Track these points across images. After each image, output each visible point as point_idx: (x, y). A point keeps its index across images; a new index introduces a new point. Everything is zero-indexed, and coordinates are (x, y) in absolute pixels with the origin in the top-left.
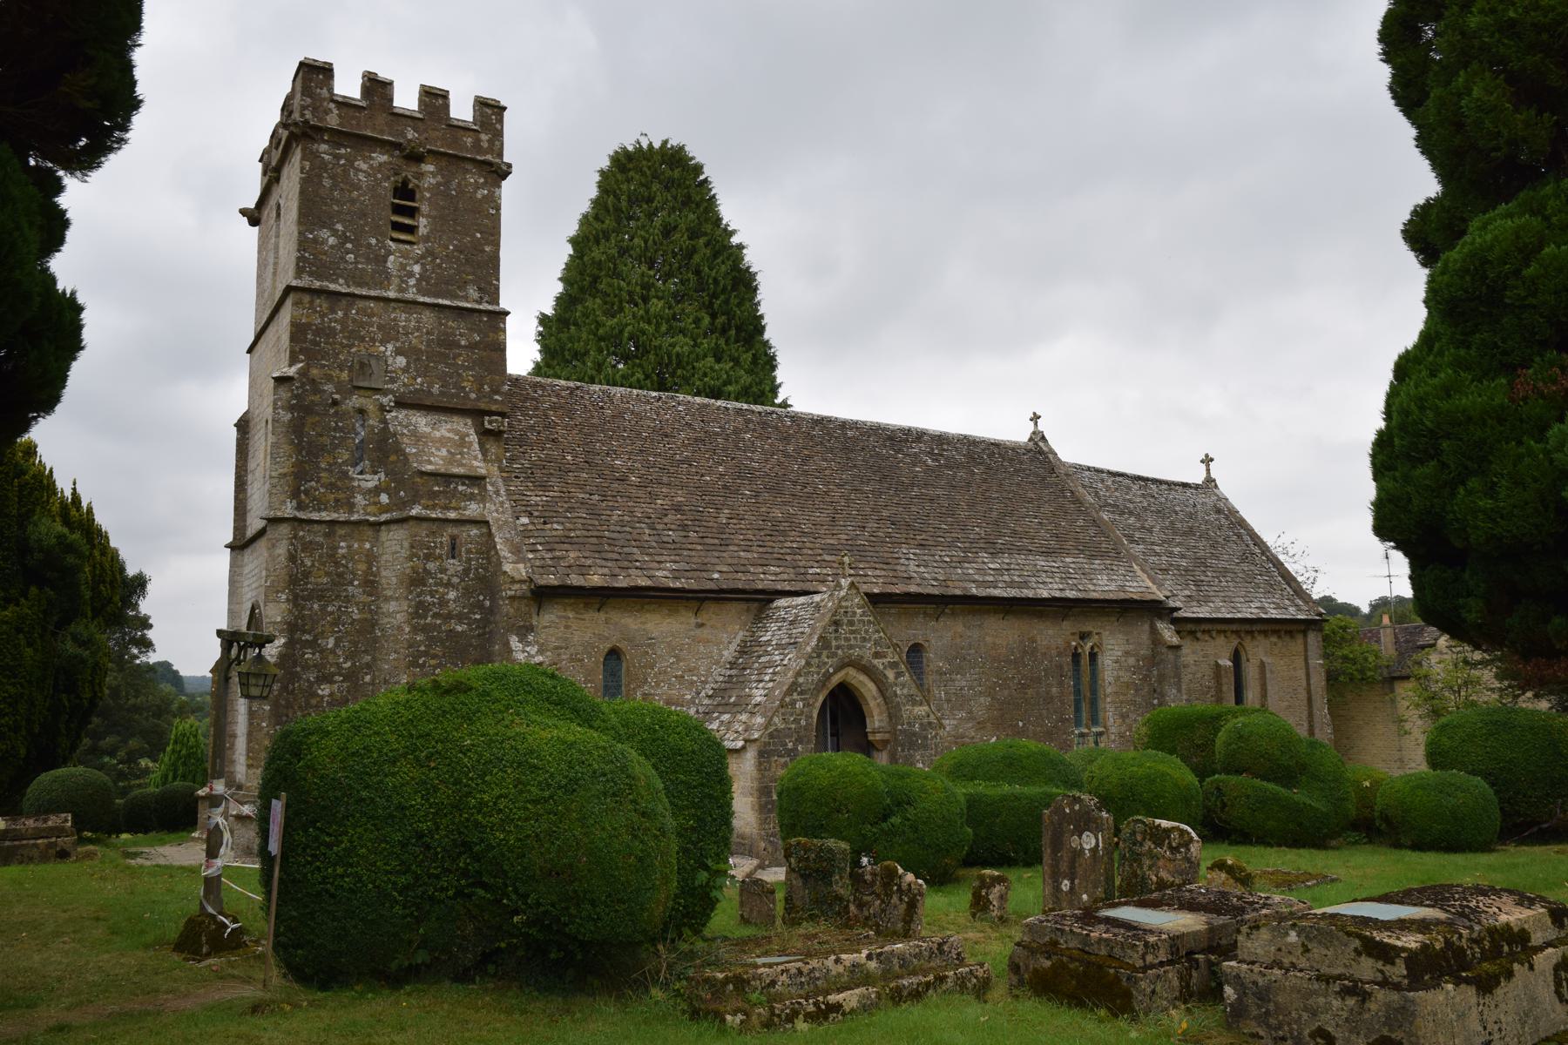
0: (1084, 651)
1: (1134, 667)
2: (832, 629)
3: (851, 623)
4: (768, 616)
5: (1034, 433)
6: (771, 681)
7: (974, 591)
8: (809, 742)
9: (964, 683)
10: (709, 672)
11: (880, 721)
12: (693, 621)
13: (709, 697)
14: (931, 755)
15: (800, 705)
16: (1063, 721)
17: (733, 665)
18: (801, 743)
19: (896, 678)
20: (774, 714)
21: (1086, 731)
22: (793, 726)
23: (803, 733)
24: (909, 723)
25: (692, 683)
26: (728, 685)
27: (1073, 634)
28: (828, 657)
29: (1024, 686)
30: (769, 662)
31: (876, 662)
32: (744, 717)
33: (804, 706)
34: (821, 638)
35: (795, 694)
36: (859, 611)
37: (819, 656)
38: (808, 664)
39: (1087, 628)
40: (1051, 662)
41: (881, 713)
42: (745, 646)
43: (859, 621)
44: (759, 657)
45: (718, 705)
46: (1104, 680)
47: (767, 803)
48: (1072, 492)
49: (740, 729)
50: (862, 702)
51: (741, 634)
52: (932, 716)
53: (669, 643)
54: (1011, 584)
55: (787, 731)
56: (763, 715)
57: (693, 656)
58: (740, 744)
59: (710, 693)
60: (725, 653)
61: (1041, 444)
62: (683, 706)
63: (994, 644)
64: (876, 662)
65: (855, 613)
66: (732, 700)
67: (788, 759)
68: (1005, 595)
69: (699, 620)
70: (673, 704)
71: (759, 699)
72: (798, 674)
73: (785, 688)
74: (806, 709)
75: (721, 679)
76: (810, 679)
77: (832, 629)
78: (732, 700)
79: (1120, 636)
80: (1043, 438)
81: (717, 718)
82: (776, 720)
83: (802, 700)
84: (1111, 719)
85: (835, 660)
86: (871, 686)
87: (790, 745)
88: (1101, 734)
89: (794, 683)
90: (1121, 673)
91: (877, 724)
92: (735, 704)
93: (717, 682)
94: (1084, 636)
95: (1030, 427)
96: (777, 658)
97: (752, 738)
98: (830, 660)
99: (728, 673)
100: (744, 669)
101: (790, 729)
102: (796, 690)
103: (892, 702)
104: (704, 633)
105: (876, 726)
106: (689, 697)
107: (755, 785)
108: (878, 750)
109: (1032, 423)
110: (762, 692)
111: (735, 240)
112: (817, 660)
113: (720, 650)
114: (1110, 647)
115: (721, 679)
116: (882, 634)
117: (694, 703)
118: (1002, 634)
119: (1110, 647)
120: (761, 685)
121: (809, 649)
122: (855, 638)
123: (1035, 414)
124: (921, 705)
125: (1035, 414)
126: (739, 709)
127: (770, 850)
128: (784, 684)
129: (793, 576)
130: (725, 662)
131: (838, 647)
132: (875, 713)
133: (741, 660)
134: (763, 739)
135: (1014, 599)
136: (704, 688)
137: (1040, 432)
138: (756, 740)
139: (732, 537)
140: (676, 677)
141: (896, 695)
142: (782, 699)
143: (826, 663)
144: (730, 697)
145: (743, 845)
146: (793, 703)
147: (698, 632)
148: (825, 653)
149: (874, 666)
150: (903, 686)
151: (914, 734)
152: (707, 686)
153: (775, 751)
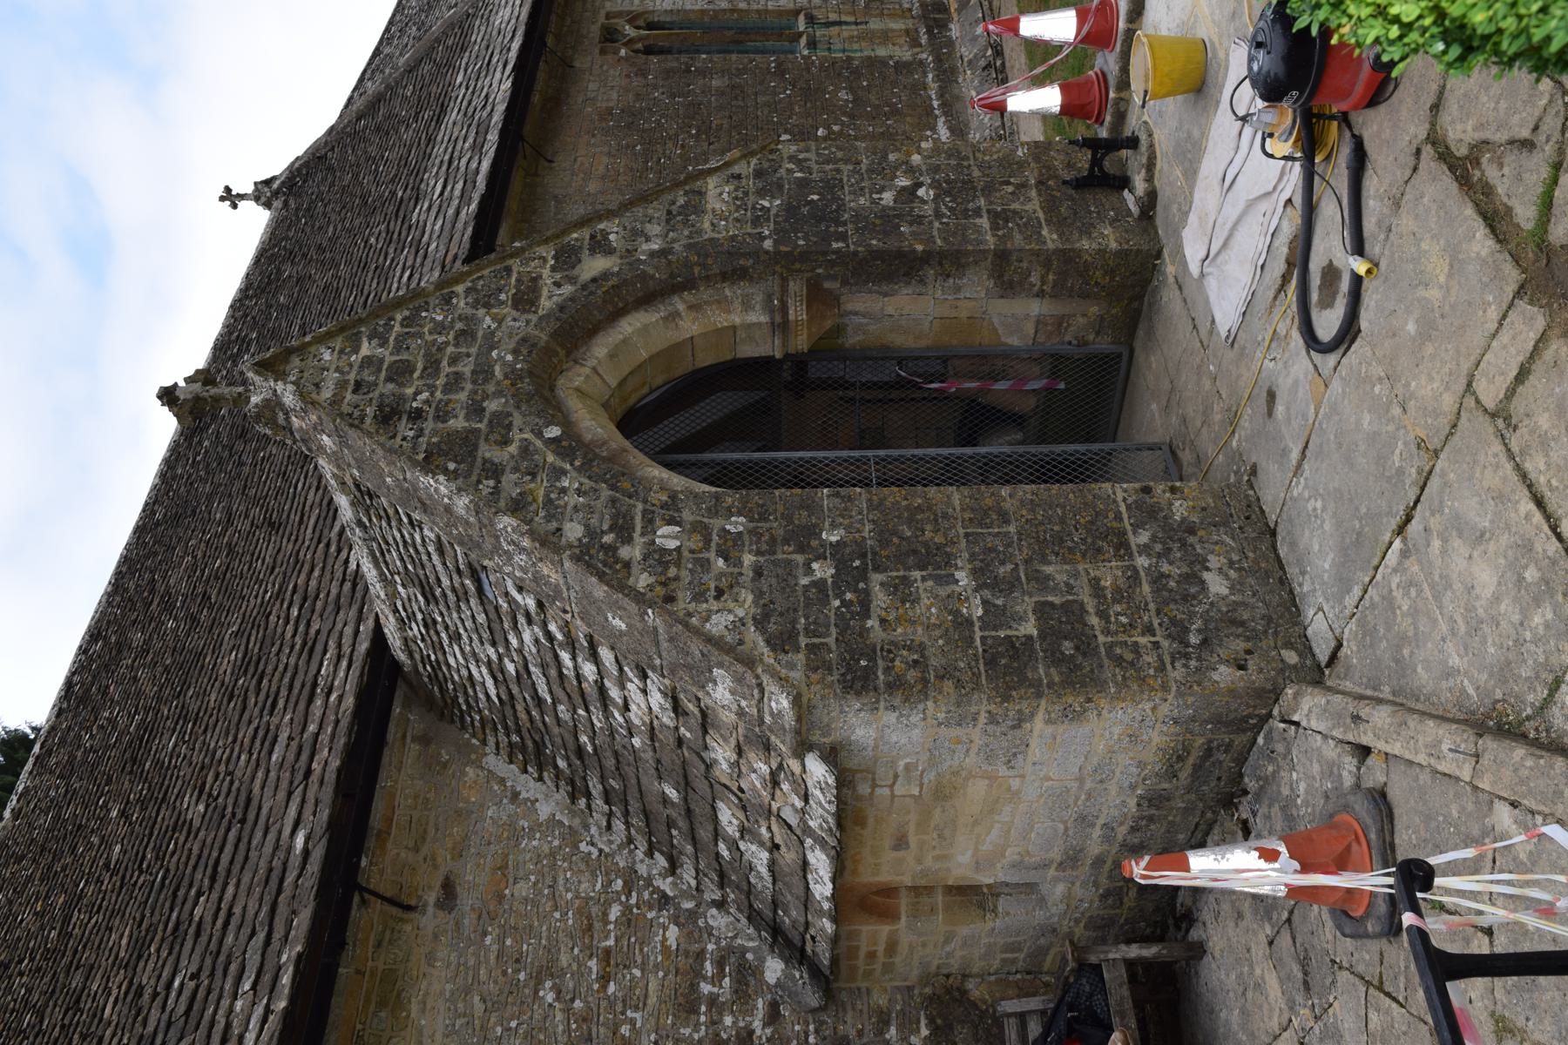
0: (640, 39)
2: (405, 429)
3: (400, 372)
4: (434, 677)
5: (257, 199)
6: (595, 657)
7: (473, 206)
8: (811, 507)
10: (600, 865)
11: (747, 306)
12: (430, 919)
13: (673, 868)
14: (854, 171)
15: (668, 537)
16: (781, 71)
17: (577, 791)
18: (813, 531)
19: (609, 251)
20: (697, 632)
21: (803, 40)
22: (748, 559)
23: (777, 527)
24: (756, 222)
25: (628, 920)
26: (634, 806)
28: (506, 442)
30: (544, 667)
31: (546, 304)
32: (722, 754)
33: (671, 521)
34: (429, 464)
35: (624, 552)
36: (365, 350)
37: (495, 471)
38: (517, 507)
40: (655, 87)
41: (724, 304)
42: (523, 748)
43: (398, 349)
44: (539, 701)
45: (694, 841)
46: (703, 12)
47: (1056, 659)
48: (359, 119)
49: (764, 768)
50: (683, 368)
51: (496, 763)
52: (736, 169)
53: (491, 1005)
54: (477, 147)
55: (764, 584)
56: (703, 678)
57: (546, 916)
58: (817, 769)
59: (661, 861)
60: (544, 810)
61: (275, 186)
62: (701, 955)
63: (603, 178)
64: (546, 304)
65: (368, 361)
66: (672, 793)
67: (877, 578)
69: (431, 898)
70: (694, 987)
71: (656, 699)
72: (549, 542)
73: (599, 591)
74: (687, 516)
75: (618, 825)
76: (573, 499)
77: (405, 429)
78: (672, 793)
80: (268, 182)
81: (733, 846)
82: (718, 624)
83: (649, 525)
85: (517, 420)
86: (629, 325)
87: (823, 570)
88: (811, 19)
89: (584, 555)
91: (758, 317)
92: (685, 785)
93: (630, 840)
94: (610, 36)
95: (247, 206)
96: (527, 636)
97: (789, 719)
98: (517, 436)
99: (599, 802)
100: (580, 751)
101: (758, 572)
102: (611, 549)
103: (687, 264)
104: (474, 878)
105: (764, 319)
106: (673, 933)
107: (982, 706)
108: (839, 330)
109: (242, 204)
110: (633, 688)
112: (509, 478)
113: (536, 826)
115: (618, 825)
116: (460, 289)
117: (693, 915)
120: (614, 693)
121: (462, 503)
122: (454, 360)
123: (222, 199)
124: (701, 194)
125: (222, 199)
126: (697, 770)
127: (1240, 645)
128: (587, 596)
129: (353, 613)
130: (573, 814)
131: (476, 410)
132: (721, 320)
133: (562, 764)
134: (797, 675)
136: (649, 881)
137: (256, 189)
138: (797, 701)
139: (236, 784)
140: (604, 979)
141: (663, 253)
142: (639, 598)
143: (526, 449)
144: (665, 800)
145: (1209, 752)
146: (658, 558)
147: (467, 901)
148: (487, 451)
149: (561, 308)
150: (636, 234)
151: (790, 210)
152: (642, 870)
153: (843, 629)
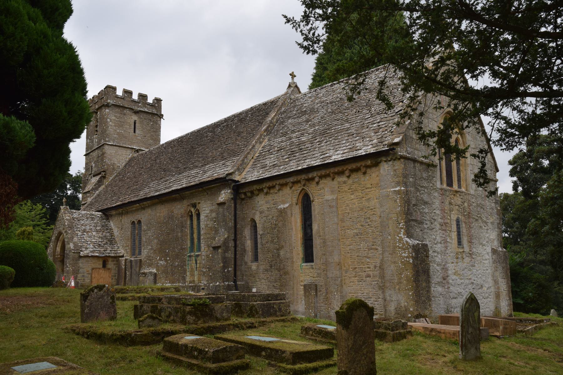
1: (215, 218)
9: (150, 234)
27: (189, 205)
29: (169, 234)
39: (194, 201)
40: (178, 221)
68: (165, 192)
79: (209, 202)
84: (203, 248)
88: (198, 256)
90: (208, 223)
111: (316, 61)
114: (204, 209)
118: (161, 211)
119: (204, 209)
135: (158, 195)
